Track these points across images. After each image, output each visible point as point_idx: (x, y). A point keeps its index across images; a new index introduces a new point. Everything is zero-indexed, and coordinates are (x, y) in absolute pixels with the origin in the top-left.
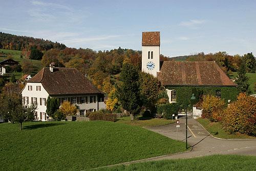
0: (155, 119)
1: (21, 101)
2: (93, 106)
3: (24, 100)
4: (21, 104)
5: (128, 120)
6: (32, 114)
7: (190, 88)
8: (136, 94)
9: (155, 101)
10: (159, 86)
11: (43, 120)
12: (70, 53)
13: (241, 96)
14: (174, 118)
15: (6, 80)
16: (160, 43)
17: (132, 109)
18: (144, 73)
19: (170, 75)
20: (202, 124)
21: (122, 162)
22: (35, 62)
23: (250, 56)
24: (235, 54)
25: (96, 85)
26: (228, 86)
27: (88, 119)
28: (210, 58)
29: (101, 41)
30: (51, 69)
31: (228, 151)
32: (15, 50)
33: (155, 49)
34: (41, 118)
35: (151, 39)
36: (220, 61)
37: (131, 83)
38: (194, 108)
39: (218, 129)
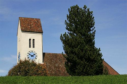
19: (57, 68)
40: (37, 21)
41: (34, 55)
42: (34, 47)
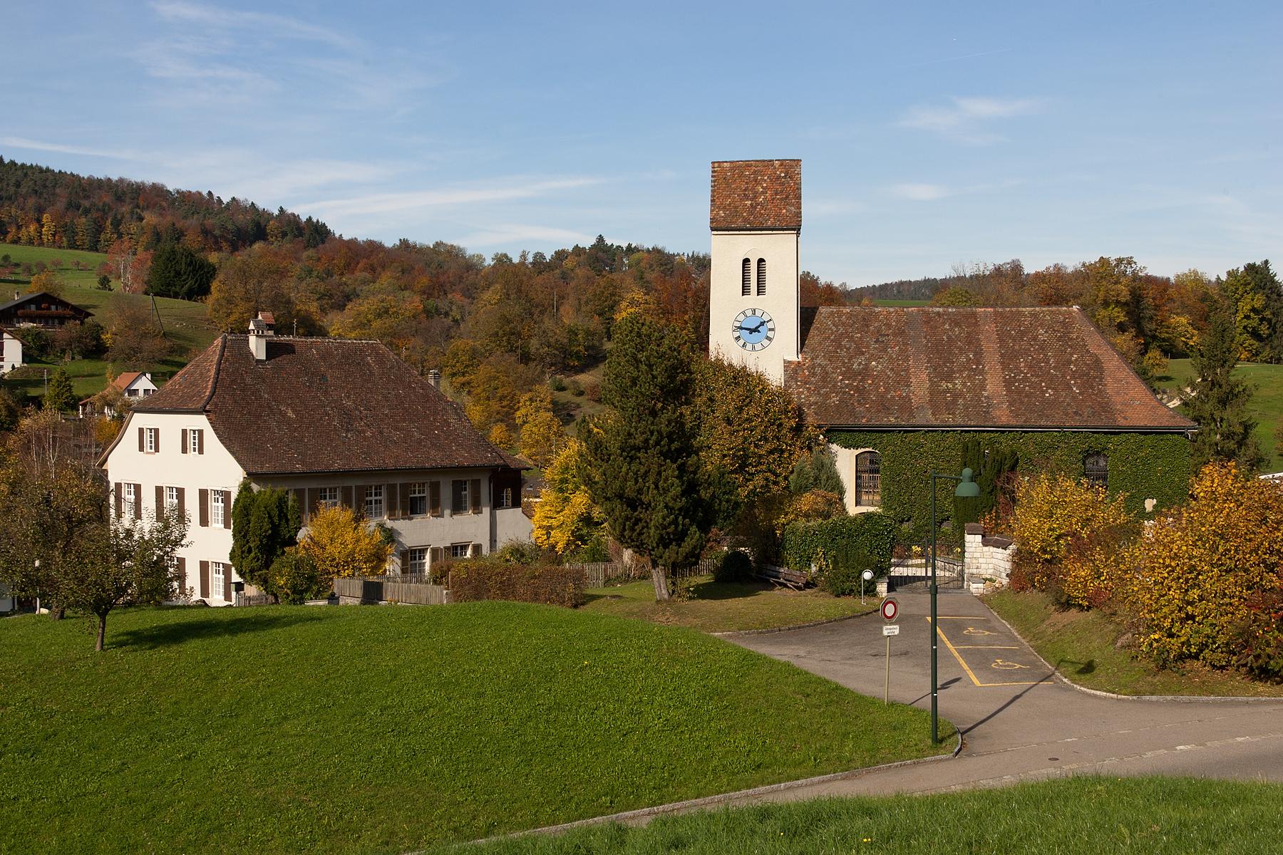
0: (777, 592)
1: (100, 506)
2: (468, 527)
3: (119, 499)
4: (102, 518)
5: (638, 595)
6: (158, 568)
7: (950, 440)
8: (682, 469)
9: (773, 504)
10: (798, 429)
11: (217, 599)
12: (349, 267)
13: (1213, 479)
14: (870, 589)
15: (27, 401)
16: (799, 215)
17: (664, 542)
18: (719, 367)
19: (850, 374)
20: (1018, 618)
21: (611, 807)
22: (173, 311)
23: (1258, 276)
24: (1051, 264)
25: (485, 427)
26: (1146, 432)
27: (439, 596)
28: (1055, 288)
29: (504, 206)
30: (256, 346)
31: (1149, 754)
32: (73, 246)
33: (776, 250)
34: (205, 591)
35: (758, 197)
36: (1106, 304)
37: (653, 413)
38: (973, 542)
39: (1095, 646)
40: (787, 174)
41: (762, 324)
42: (760, 290)
